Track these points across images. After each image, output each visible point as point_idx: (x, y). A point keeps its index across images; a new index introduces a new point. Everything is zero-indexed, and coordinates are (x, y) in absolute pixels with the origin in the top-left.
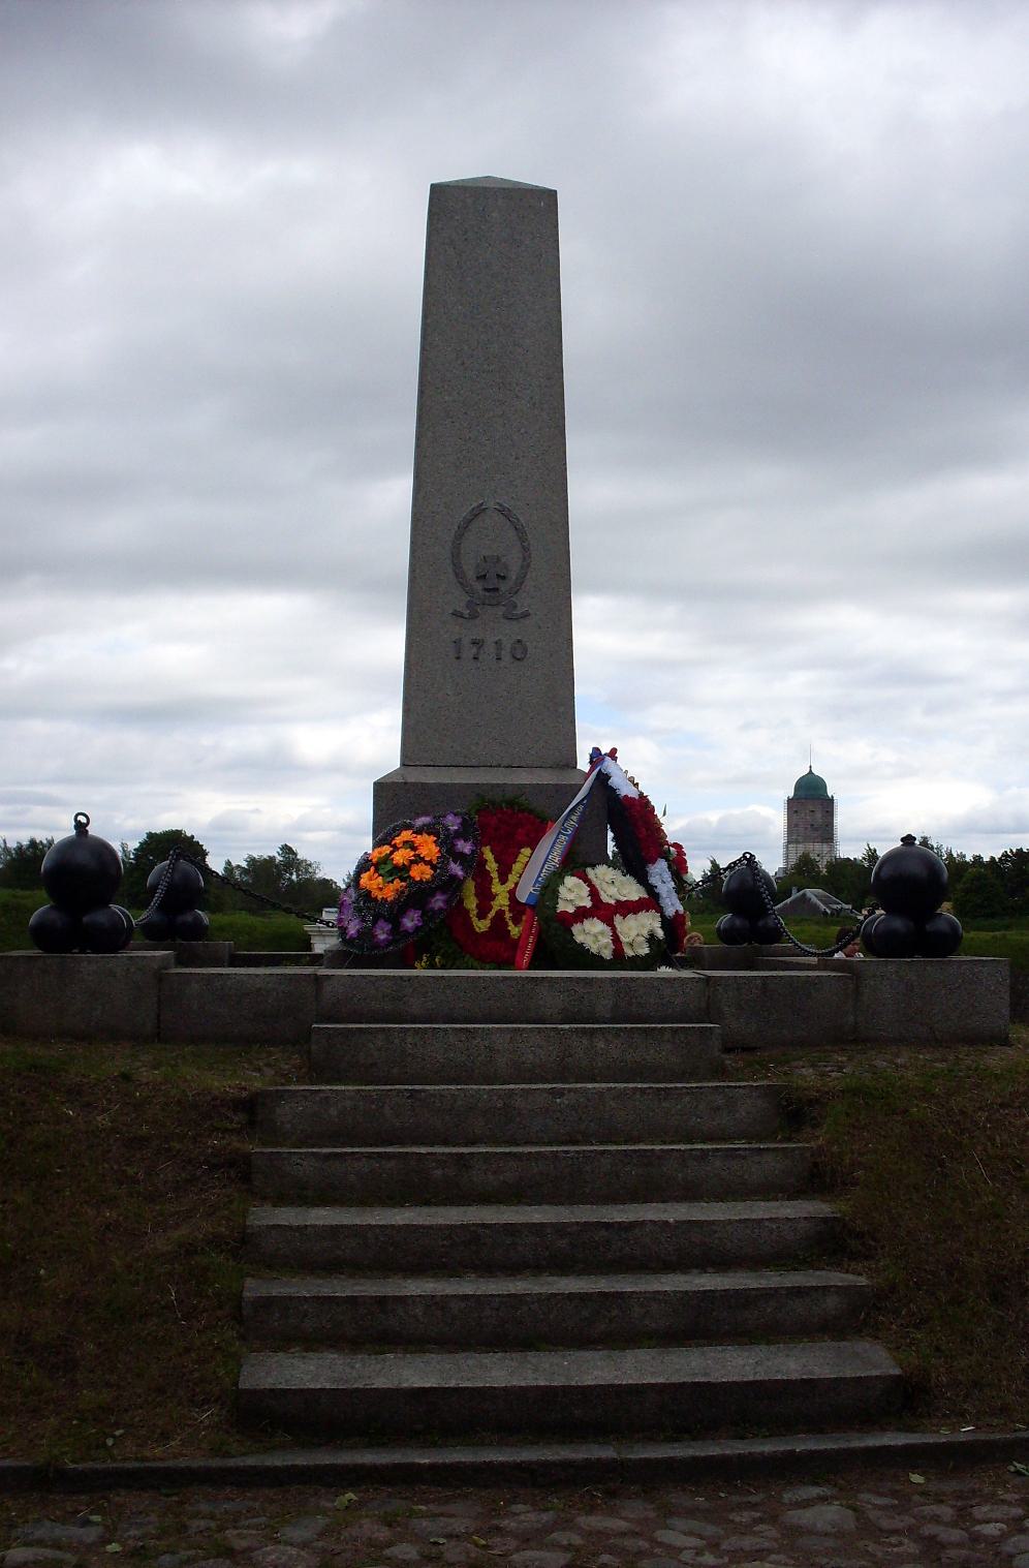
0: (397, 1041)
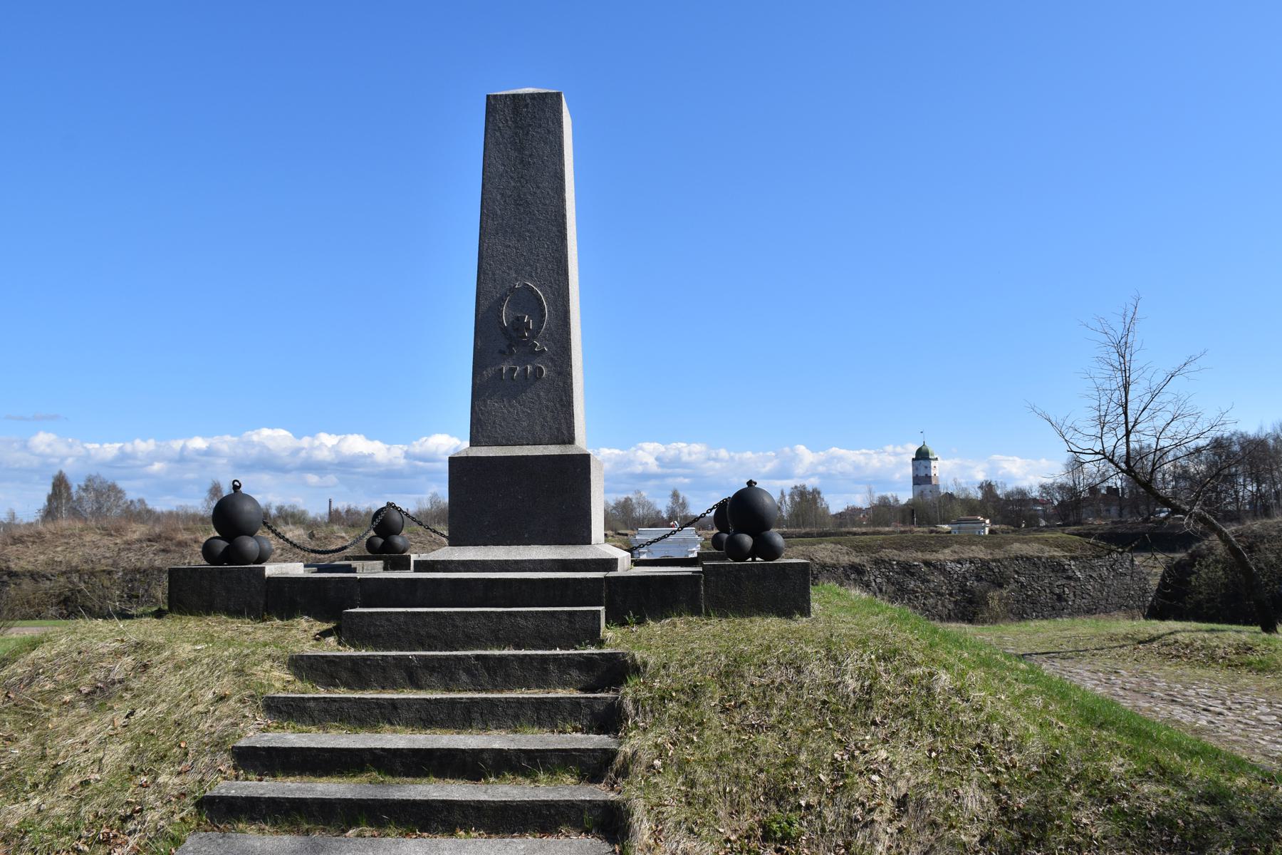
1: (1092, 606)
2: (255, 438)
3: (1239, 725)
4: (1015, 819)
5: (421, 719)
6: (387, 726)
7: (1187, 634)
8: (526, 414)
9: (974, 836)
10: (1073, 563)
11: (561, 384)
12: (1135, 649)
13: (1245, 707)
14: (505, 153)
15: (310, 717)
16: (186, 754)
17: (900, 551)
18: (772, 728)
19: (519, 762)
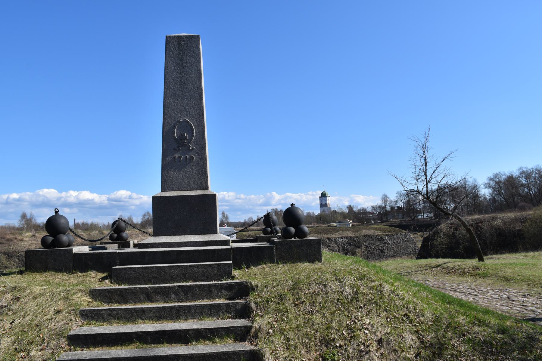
1: (394, 254)
2: (41, 193)
3: (485, 299)
4: (428, 346)
5: (156, 317)
6: (140, 321)
7: (452, 263)
8: (186, 177)
9: (412, 354)
10: (387, 237)
11: (202, 163)
12: (431, 270)
13: (484, 292)
14: (174, 62)
15: (103, 318)
16: (44, 340)
17: (318, 234)
18: (318, 312)
19: (206, 334)
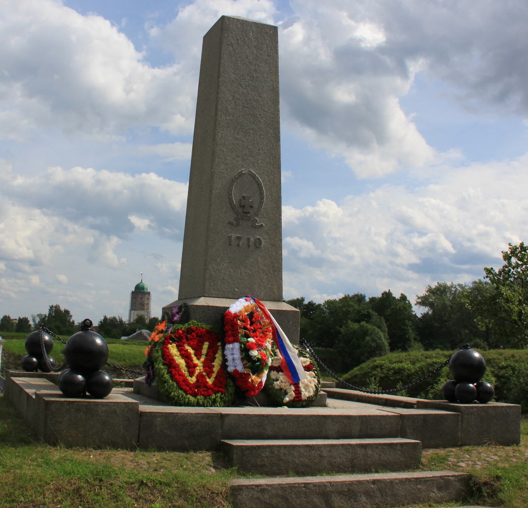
0: (276, 452)
11: (274, 254)
